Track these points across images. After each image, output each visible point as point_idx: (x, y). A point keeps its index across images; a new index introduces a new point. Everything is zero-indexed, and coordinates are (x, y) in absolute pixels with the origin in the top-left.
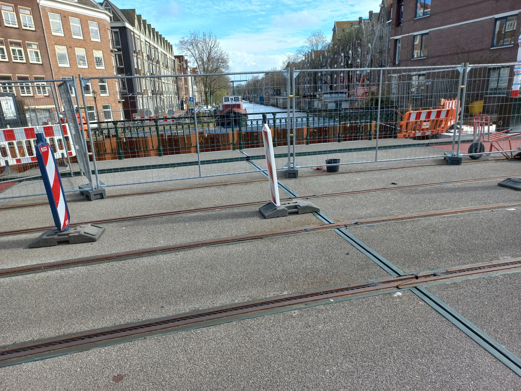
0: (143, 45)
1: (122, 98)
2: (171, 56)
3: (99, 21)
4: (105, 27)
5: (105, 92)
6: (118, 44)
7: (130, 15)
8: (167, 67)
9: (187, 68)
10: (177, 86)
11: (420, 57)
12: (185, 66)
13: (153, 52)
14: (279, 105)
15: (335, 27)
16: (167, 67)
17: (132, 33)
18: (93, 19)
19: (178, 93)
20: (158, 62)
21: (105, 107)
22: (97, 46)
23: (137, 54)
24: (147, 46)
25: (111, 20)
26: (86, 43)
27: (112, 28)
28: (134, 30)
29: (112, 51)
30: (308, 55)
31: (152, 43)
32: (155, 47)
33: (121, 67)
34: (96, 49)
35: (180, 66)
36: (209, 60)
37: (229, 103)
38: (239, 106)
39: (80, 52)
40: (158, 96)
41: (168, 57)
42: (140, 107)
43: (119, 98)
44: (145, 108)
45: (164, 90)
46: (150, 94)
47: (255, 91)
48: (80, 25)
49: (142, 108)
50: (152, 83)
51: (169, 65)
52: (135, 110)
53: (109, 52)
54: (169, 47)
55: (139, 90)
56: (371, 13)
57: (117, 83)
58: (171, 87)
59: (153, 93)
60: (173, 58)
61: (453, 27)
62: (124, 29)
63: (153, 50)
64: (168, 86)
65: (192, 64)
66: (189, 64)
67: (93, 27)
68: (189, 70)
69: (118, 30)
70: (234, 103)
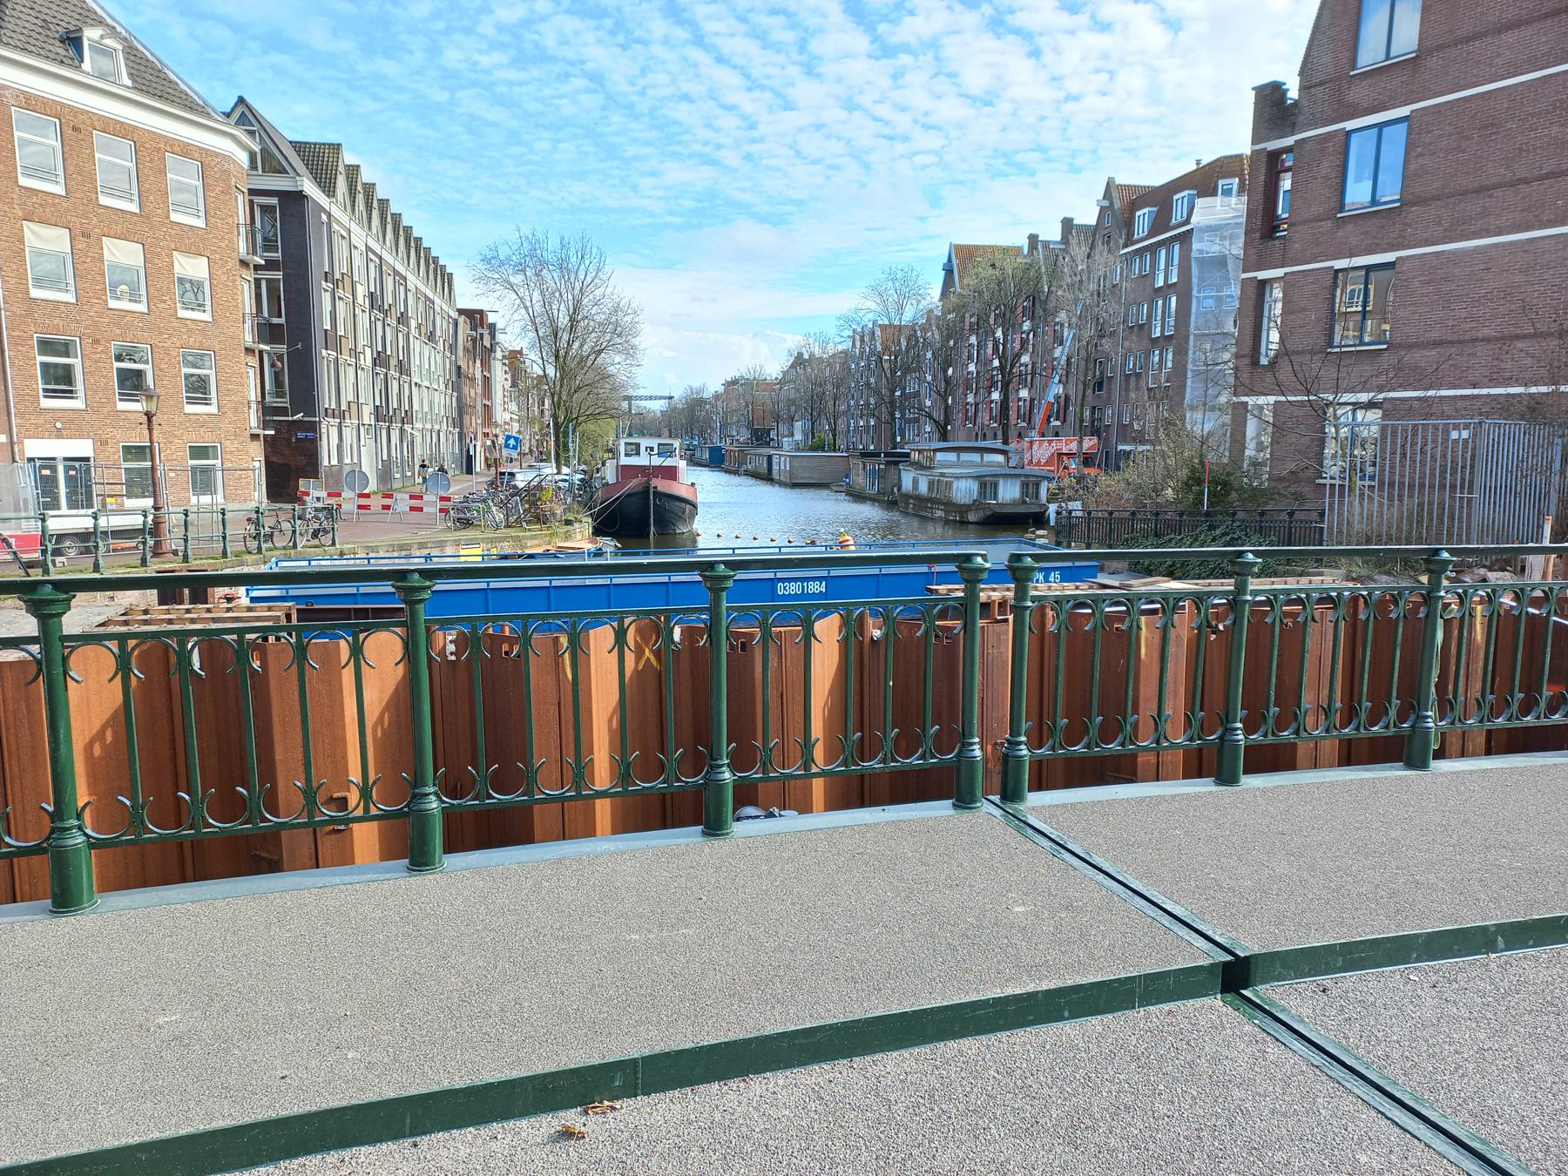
0: (358, 261)
1: (265, 426)
2: (445, 307)
3: (208, 163)
4: (227, 181)
5: (206, 401)
6: (269, 245)
7: (321, 160)
8: (431, 337)
9: (492, 350)
10: (459, 399)
11: (1362, 343)
12: (487, 343)
13: (390, 288)
14: (775, 475)
15: (950, 260)
16: (431, 337)
17: (324, 217)
18: (185, 150)
19: (459, 421)
20: (403, 319)
21: (199, 452)
22: (191, 242)
23: (336, 283)
24: (372, 266)
25: (253, 166)
26: (147, 226)
27: (252, 192)
28: (331, 207)
29: (244, 263)
30: (863, 336)
31: (386, 256)
32: (396, 273)
33: (276, 321)
34: (186, 251)
35: (474, 340)
36: (573, 321)
37: (642, 460)
38: (671, 473)
39: (122, 254)
40: (396, 426)
41: (437, 308)
42: (328, 456)
43: (254, 423)
44: (347, 461)
45: (416, 407)
46: (368, 418)
47: (737, 431)
48: (132, 165)
49: (334, 462)
50: (379, 385)
51: (438, 333)
52: (311, 467)
53: (233, 263)
54: (444, 279)
55: (327, 400)
56: (1067, 224)
57: (251, 372)
58: (438, 399)
59: (379, 414)
60: (454, 315)
61: (1476, 250)
62: (294, 200)
63: (389, 282)
64: (430, 399)
65: (513, 334)
66: (500, 337)
67: (182, 177)
68: (499, 354)
69: (274, 201)
70: (657, 461)
